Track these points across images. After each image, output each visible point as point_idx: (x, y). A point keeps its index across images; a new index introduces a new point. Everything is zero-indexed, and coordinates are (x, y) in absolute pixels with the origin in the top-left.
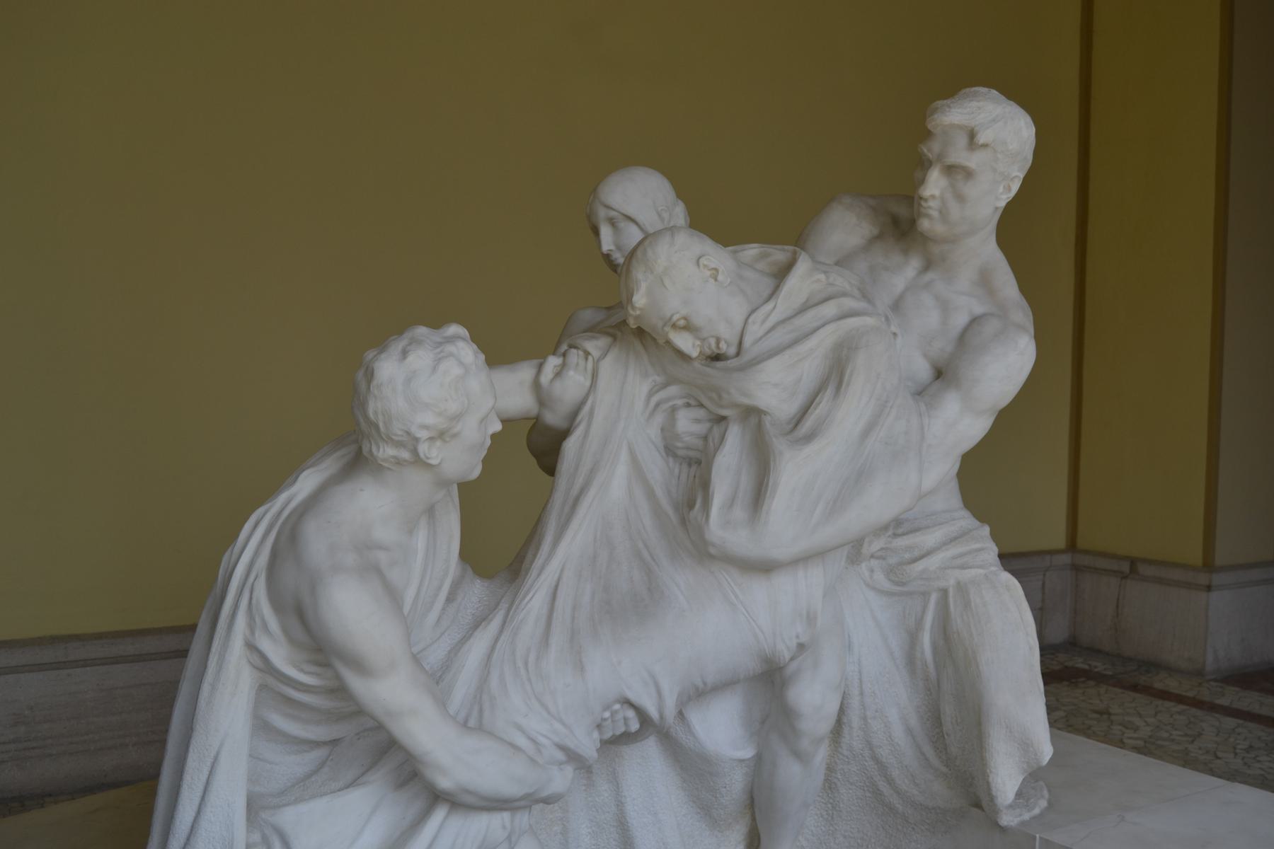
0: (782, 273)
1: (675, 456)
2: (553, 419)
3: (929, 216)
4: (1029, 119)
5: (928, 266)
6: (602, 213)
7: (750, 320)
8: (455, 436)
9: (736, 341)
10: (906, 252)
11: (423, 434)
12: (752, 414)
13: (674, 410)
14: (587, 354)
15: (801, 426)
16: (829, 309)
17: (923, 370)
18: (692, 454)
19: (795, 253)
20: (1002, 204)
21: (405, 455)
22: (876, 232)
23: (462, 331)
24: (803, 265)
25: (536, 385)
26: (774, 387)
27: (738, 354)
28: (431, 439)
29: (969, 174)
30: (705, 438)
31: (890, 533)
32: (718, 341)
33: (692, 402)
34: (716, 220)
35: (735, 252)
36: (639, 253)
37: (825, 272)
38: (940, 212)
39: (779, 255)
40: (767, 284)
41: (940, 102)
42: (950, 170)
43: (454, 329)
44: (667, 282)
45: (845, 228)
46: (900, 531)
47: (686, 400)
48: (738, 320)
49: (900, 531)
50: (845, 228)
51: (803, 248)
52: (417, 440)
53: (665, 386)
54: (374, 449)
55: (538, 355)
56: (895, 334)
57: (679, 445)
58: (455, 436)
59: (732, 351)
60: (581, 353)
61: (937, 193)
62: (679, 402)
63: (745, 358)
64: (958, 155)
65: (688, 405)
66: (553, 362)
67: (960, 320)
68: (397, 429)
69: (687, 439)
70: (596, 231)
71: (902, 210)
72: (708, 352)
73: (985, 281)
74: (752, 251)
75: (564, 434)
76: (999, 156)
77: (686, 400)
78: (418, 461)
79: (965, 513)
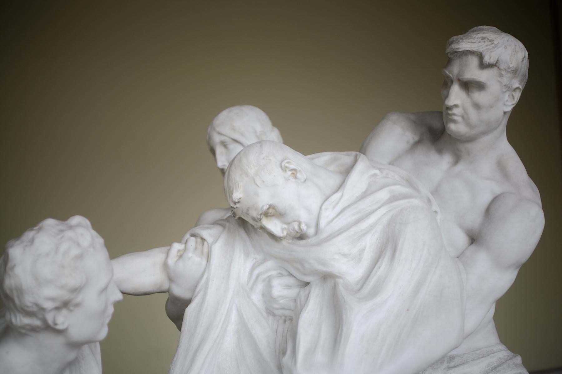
0: (347, 171)
1: (274, 315)
2: (179, 291)
3: (454, 121)
4: (521, 45)
5: (457, 159)
6: (217, 139)
7: (324, 207)
8: (77, 305)
9: (313, 224)
10: (440, 151)
11: (48, 305)
12: (327, 277)
13: (270, 279)
14: (203, 240)
15: (369, 288)
16: (383, 195)
17: (462, 239)
18: (287, 313)
19: (356, 156)
20: (509, 109)
21: (37, 323)
22: (417, 138)
23: (86, 222)
24: (362, 164)
25: (165, 266)
26: (346, 259)
27: (316, 233)
28: (58, 309)
29: (480, 86)
30: (295, 300)
31: (445, 365)
32: (300, 223)
33: (285, 273)
34: (302, 139)
35: (313, 159)
36: (236, 162)
37: (379, 169)
38: (463, 117)
39: (345, 158)
40: (334, 180)
41: (455, 38)
42: (467, 86)
43: (76, 220)
44: (258, 181)
45: (394, 135)
46: (452, 364)
47: (279, 271)
48: (315, 208)
49: (452, 364)
50: (394, 135)
51: (364, 153)
52: (43, 309)
53: (264, 261)
54: (13, 320)
55: (165, 242)
56: (436, 212)
57: (276, 306)
58: (77, 305)
59: (311, 231)
60: (199, 240)
61: (458, 102)
62: (274, 273)
63: (323, 236)
64: (473, 72)
65: (281, 275)
66: (177, 247)
67: (485, 198)
68: (28, 300)
69: (282, 301)
70: (213, 151)
71: (436, 124)
72: (293, 233)
73: (501, 167)
74: (325, 157)
75: (187, 303)
76: (503, 73)
77: (279, 271)
78: (49, 328)
79: (502, 347)
